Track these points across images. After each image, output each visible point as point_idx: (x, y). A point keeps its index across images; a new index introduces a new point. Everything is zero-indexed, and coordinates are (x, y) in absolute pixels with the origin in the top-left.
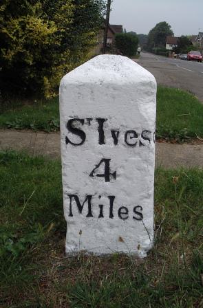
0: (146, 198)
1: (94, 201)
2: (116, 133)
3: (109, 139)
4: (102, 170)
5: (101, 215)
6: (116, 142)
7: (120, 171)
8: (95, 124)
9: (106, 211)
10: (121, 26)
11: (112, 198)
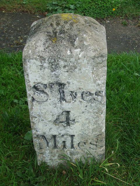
1: (60, 141)
8: (56, 87)
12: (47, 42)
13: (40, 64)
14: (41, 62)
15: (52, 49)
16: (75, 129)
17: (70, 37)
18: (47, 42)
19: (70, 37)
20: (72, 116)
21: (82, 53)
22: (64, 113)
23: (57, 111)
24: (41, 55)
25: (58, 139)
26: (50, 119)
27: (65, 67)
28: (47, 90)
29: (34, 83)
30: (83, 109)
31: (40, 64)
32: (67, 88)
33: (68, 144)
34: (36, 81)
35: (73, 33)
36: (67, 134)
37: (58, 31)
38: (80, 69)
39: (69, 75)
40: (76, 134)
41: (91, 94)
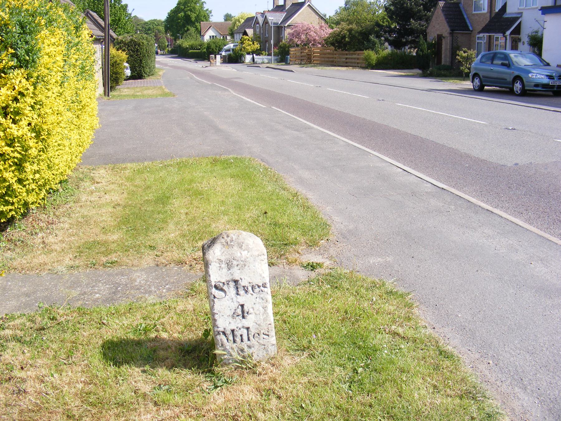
0: (398, 335)
1: (238, 333)
2: (246, 288)
3: (242, 292)
4: (239, 311)
5: (242, 341)
6: (246, 292)
7: (251, 311)
8: (232, 284)
9: (245, 338)
10: (542, 14)
11: (248, 329)
12: (222, 249)
13: (219, 266)
14: (219, 264)
15: (227, 254)
16: (249, 321)
17: (239, 244)
18: (222, 249)
19: (239, 244)
20: (246, 308)
21: (249, 254)
22: (240, 307)
23: (235, 305)
24: (219, 258)
25: (236, 333)
26: (228, 314)
27: (237, 265)
28: (225, 288)
29: (215, 282)
30: (254, 301)
31: (219, 266)
32: (240, 284)
33: (245, 338)
34: (217, 281)
35: (240, 241)
36: (243, 327)
37: (229, 241)
38: (249, 266)
39: (241, 272)
40: (250, 326)
41: (259, 287)
